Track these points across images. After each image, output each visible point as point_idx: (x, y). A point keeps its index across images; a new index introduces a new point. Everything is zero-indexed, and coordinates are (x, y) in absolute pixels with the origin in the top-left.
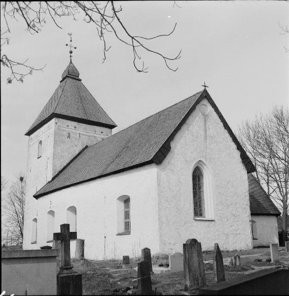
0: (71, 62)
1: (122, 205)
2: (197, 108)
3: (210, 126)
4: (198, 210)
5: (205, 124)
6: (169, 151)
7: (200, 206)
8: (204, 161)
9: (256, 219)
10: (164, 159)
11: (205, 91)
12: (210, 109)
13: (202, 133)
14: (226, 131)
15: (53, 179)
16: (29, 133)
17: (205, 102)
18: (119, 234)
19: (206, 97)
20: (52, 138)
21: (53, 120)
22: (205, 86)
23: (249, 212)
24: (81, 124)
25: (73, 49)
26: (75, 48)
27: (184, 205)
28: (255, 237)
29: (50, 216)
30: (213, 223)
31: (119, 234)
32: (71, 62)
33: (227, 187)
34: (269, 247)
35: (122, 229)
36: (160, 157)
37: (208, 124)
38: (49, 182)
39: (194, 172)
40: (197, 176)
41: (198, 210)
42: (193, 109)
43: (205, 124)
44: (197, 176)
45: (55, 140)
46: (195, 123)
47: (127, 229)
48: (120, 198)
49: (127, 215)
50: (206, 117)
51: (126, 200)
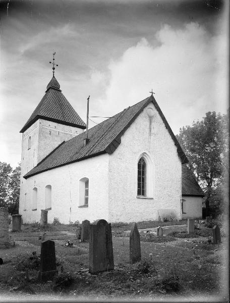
0: (54, 77)
1: (83, 185)
2: (145, 110)
3: (155, 127)
4: (141, 191)
5: (150, 124)
6: (119, 144)
7: (143, 187)
8: (148, 153)
9: (185, 198)
10: (115, 150)
11: (152, 97)
12: (154, 112)
13: (148, 131)
14: (167, 130)
15: (38, 165)
16: (23, 131)
17: (151, 106)
18: (81, 207)
19: (152, 102)
20: (37, 135)
21: (39, 121)
22: (152, 93)
23: (180, 194)
24: (59, 124)
25: (55, 66)
26: (57, 65)
27: (130, 187)
28: (184, 212)
29: (47, 189)
30: (152, 201)
31: (81, 207)
32: (54, 77)
33: (167, 174)
34: (187, 220)
35: (83, 203)
36: (111, 149)
37: (153, 124)
38: (36, 167)
39: (139, 162)
40: (142, 167)
41: (141, 191)
42: (141, 111)
43: (150, 124)
44: (142, 167)
45: (40, 136)
46: (141, 122)
47: (86, 205)
48: (82, 180)
49: (87, 192)
50: (151, 118)
51: (86, 182)
